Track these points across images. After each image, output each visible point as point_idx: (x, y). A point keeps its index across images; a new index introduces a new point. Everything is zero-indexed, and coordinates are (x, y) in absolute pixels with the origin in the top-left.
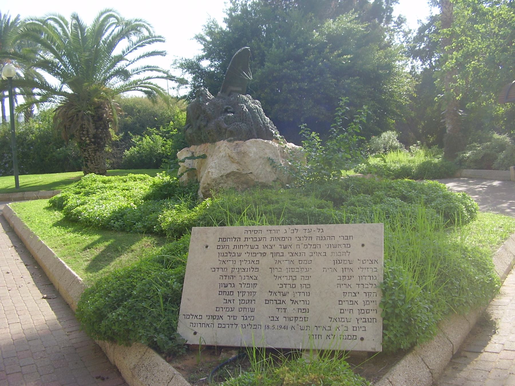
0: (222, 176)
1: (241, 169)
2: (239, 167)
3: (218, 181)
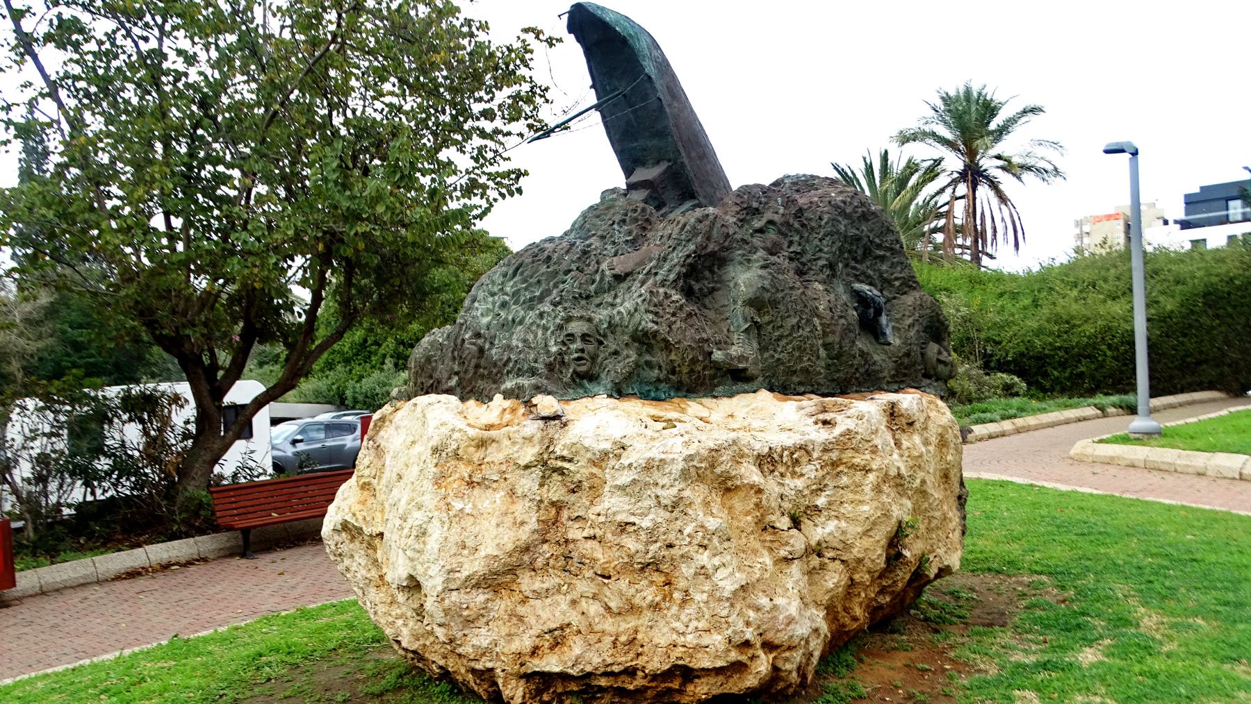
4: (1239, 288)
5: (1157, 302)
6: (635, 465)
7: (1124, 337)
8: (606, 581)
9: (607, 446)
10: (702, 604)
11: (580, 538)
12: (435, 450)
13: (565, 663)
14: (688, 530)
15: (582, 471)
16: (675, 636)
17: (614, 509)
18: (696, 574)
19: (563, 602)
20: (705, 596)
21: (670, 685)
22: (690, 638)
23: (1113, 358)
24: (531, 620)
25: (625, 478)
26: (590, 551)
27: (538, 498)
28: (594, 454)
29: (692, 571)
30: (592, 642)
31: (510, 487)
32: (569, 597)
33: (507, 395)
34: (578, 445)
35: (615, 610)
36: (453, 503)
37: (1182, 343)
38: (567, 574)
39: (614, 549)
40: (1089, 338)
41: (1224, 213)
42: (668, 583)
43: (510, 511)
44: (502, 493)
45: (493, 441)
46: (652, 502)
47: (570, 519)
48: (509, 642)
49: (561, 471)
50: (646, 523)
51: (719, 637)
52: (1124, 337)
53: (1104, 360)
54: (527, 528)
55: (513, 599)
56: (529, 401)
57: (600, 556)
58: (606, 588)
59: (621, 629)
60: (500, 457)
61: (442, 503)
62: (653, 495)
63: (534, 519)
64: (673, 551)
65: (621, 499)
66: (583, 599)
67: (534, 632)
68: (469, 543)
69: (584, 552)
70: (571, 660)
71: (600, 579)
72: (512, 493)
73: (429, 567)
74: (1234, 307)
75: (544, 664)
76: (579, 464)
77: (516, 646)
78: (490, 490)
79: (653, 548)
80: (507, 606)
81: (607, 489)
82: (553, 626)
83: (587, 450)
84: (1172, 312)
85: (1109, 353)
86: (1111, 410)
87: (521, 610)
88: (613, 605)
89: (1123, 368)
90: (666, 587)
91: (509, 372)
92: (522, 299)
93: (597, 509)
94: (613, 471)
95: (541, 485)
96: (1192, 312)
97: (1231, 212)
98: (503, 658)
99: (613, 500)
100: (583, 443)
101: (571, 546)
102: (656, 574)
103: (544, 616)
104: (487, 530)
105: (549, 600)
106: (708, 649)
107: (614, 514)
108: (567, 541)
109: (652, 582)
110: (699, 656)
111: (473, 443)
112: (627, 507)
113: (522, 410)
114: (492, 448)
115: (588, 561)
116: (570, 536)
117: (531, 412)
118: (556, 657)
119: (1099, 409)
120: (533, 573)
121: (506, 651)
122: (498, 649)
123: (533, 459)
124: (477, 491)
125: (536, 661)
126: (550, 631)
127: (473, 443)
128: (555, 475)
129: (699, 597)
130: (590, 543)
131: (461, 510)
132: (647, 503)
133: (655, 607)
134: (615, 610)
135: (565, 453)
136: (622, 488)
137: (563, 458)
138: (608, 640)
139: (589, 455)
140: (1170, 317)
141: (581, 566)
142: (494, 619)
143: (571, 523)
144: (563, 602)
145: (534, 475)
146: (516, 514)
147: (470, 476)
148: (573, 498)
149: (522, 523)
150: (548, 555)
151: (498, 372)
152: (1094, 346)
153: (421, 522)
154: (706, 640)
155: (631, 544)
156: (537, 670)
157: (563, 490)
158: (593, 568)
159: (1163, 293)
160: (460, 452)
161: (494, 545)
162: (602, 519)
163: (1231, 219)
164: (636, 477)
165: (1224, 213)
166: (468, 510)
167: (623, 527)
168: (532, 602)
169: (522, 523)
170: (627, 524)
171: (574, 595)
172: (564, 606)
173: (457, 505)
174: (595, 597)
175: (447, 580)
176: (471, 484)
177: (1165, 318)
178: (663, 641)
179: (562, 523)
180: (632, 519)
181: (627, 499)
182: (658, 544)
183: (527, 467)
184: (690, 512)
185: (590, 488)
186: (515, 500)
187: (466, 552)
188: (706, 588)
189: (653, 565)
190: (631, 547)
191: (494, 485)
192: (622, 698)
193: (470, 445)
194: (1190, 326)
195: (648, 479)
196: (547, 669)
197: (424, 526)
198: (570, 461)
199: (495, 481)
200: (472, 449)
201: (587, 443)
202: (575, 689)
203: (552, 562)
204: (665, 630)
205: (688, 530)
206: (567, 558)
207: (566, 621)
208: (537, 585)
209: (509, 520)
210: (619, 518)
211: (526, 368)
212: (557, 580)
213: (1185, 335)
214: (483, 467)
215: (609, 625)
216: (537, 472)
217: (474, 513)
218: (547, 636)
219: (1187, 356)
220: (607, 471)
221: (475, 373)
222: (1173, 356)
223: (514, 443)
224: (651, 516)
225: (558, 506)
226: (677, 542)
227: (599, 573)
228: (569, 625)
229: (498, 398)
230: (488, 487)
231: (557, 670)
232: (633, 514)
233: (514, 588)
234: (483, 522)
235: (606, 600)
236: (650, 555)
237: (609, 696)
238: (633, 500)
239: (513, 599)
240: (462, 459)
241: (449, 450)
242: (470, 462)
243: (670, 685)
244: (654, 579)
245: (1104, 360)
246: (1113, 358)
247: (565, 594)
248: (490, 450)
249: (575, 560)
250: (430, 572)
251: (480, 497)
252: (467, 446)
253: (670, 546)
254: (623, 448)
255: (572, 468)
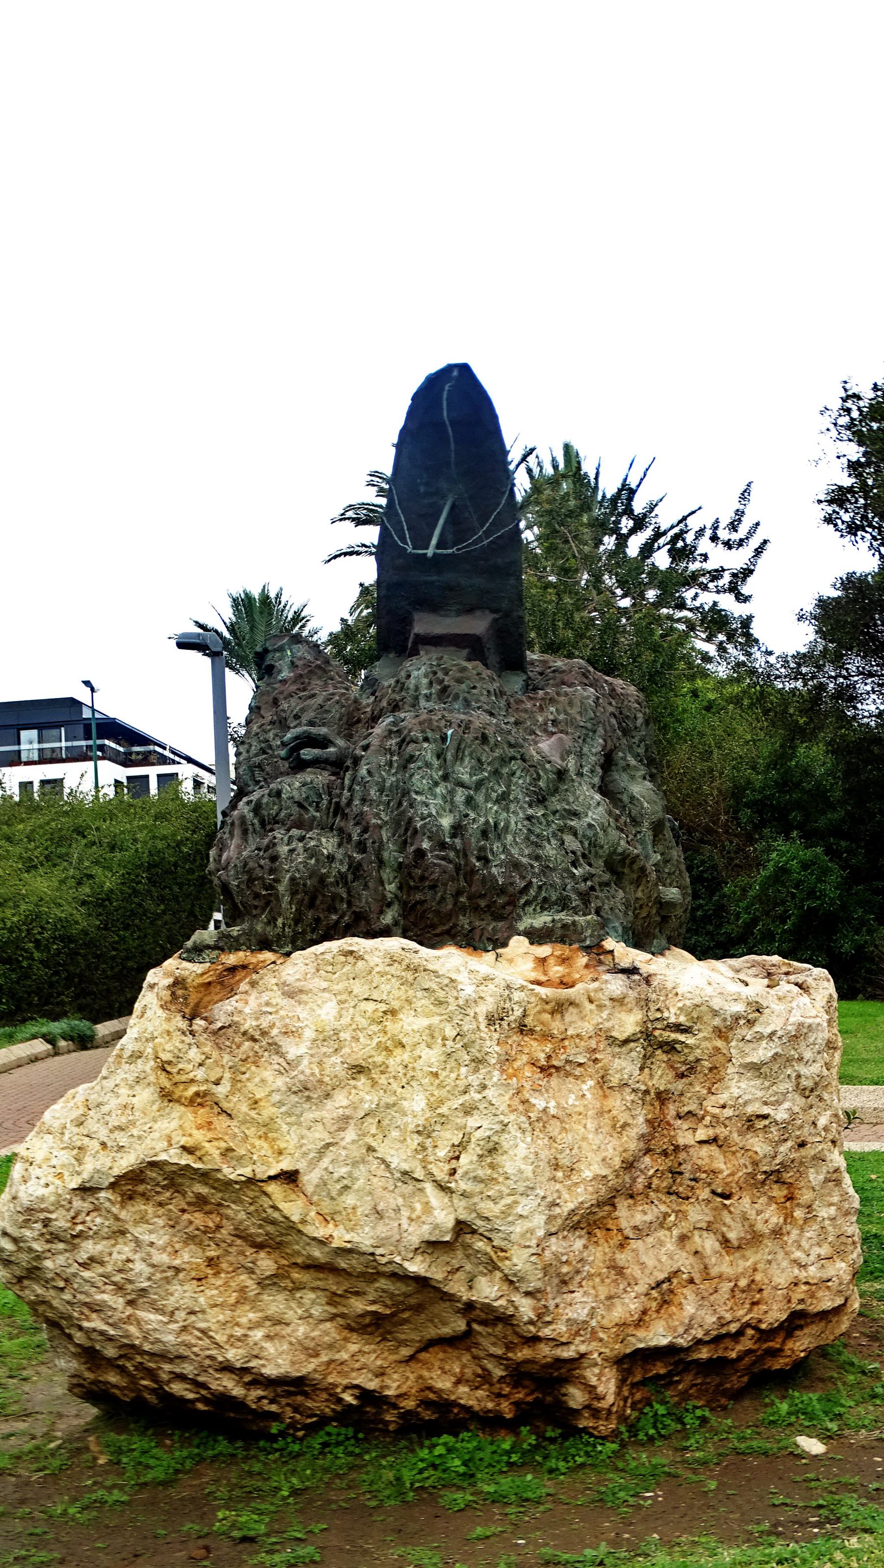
0: (85, 1190)
1: (213, 1150)
2: (199, 1136)
3: (60, 1220)
4: (186, 858)
5: (90, 877)
6: (780, 1033)
7: (56, 929)
8: (727, 1202)
9: (739, 1008)
10: (827, 1222)
11: (693, 1143)
12: (491, 1020)
13: (675, 1331)
14: (822, 1121)
15: (705, 1044)
16: (796, 1271)
17: (746, 1097)
18: (827, 1180)
19: (668, 1240)
20: (832, 1210)
21: (771, 1344)
22: (812, 1269)
23: (42, 962)
24: (634, 1270)
25: (762, 1053)
26: (707, 1160)
27: (643, 1088)
28: (725, 1020)
29: (821, 1177)
30: (705, 1294)
31: (602, 1073)
32: (676, 1232)
33: (536, 937)
34: (703, 1008)
35: (736, 1243)
36: (533, 1100)
37: (123, 939)
38: (674, 1197)
39: (739, 1155)
40: (11, 930)
41: (16, 748)
42: (790, 1198)
43: (606, 1109)
44: (591, 1083)
45: (571, 1004)
46: (789, 1086)
47: (679, 1117)
48: (609, 1308)
49: (670, 1047)
50: (781, 1114)
51: (843, 1265)
52: (56, 929)
53: (30, 967)
54: (633, 1132)
55: (612, 1242)
56: (599, 946)
57: (723, 1166)
58: (725, 1213)
59: (740, 1270)
60: (586, 1027)
61: (516, 1102)
62: (794, 1075)
63: (641, 1119)
64: (803, 1152)
65: (752, 1083)
66: (696, 1233)
67: (641, 1288)
68: (565, 1161)
69: (700, 1162)
70: (682, 1323)
71: (719, 1199)
72: (602, 1079)
73: (516, 1202)
74: (181, 885)
75: (651, 1335)
76: (701, 1035)
77: (618, 1313)
78: (571, 1079)
79: (783, 1148)
80: (605, 1254)
81: (731, 1070)
82: (661, 1276)
83: (715, 1013)
84: (111, 891)
85: (37, 955)
86: (62, 1043)
87: (622, 1258)
88: (732, 1236)
89: (55, 979)
90: (788, 1204)
91: (528, 903)
92: (494, 795)
93: (723, 1098)
94: (741, 1044)
95: (642, 1069)
96: (135, 892)
97: (24, 746)
98: (601, 1335)
99: (743, 1085)
100: (711, 1004)
101: (682, 1156)
102: (775, 1186)
103: (650, 1262)
104: (584, 1139)
105: (650, 1240)
106: (830, 1284)
107: (746, 1103)
108: (677, 1148)
109: (771, 1198)
110: (820, 1294)
111: (548, 1007)
112: (760, 1094)
113: (582, 959)
114: (571, 1014)
115: (704, 1176)
116: (681, 1141)
117: (600, 962)
118: (662, 1323)
119: (49, 1042)
120: (630, 1201)
121: (605, 1322)
122: (593, 1323)
123: (638, 1029)
124: (554, 1081)
125: (641, 1333)
126: (659, 1284)
127: (548, 1007)
128: (659, 1052)
129: (824, 1213)
130: (705, 1151)
131: (545, 1110)
132: (782, 1087)
133: (777, 1233)
134: (736, 1243)
135: (682, 1019)
136: (756, 1068)
137: (678, 1028)
138: (726, 1286)
139: (717, 1022)
140: (109, 900)
141: (693, 1183)
142: (590, 1276)
143: (680, 1122)
144: (668, 1240)
145: (634, 1054)
146: (614, 1112)
147: (549, 1057)
148: (680, 1085)
149: (625, 1125)
150: (651, 1172)
151: (509, 903)
152: (17, 944)
153: (488, 1133)
154: (830, 1272)
155: (759, 1145)
156: (641, 1345)
157: (671, 1075)
158: (709, 1184)
159: (97, 863)
160: (529, 1021)
161: (599, 1159)
162: (728, 1112)
163: (24, 758)
164: (779, 1050)
165: (16, 748)
166: (553, 1111)
167: (751, 1123)
168: (634, 1244)
169: (625, 1125)
170: (758, 1116)
171: (684, 1227)
172: (670, 1246)
173: (539, 1102)
174: (709, 1228)
175: (550, 1219)
176: (547, 1070)
177: (103, 900)
178: (782, 1280)
179: (668, 1124)
180: (766, 1110)
181: (758, 1082)
182: (789, 1144)
183: (626, 1042)
184: (826, 1096)
185: (711, 1070)
186: (608, 1091)
187: (560, 1174)
188: (835, 1199)
189: (776, 1176)
190: (758, 1149)
191: (578, 1071)
192: (706, 1376)
193: (544, 1011)
194: (133, 913)
195: (793, 1052)
196: (653, 1343)
197: (495, 1138)
198: (686, 1030)
199: (580, 1065)
200: (546, 1017)
201: (716, 1003)
202: (662, 1371)
203: (655, 1181)
204: (785, 1264)
205: (822, 1121)
206: (676, 1173)
207: (674, 1269)
208: (639, 1218)
209: (606, 1121)
210: (750, 1110)
211: (554, 898)
212: (663, 1208)
213: (127, 927)
214: (566, 1043)
215: (724, 1266)
216: (638, 1049)
217: (561, 1114)
218: (654, 1293)
219: (127, 958)
220: (733, 1044)
221: (455, 904)
222: (113, 958)
223: (600, 1007)
224: (786, 1105)
225: (662, 1097)
226: (810, 1139)
227: (719, 1190)
228: (677, 1273)
229: (518, 944)
230: (568, 1074)
231: (664, 1342)
232: (766, 1103)
233: (609, 1226)
234: (576, 1127)
235: (725, 1229)
236: (777, 1161)
237: (690, 1378)
238: (767, 1084)
239: (612, 1242)
240: (532, 1031)
241: (512, 1018)
242: (547, 1036)
243: (771, 1344)
244: (774, 1194)
245: (30, 967)
246: (42, 962)
247: (669, 1229)
248: (568, 1018)
249: (687, 1175)
250: (519, 1210)
251: (560, 1090)
252: (539, 1012)
253: (802, 1145)
254: (758, 1010)
255: (690, 1041)
